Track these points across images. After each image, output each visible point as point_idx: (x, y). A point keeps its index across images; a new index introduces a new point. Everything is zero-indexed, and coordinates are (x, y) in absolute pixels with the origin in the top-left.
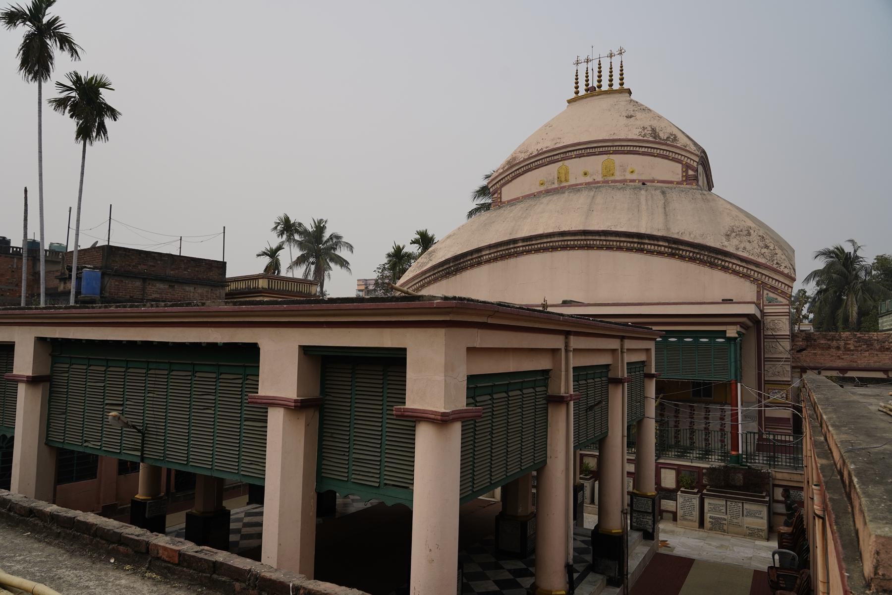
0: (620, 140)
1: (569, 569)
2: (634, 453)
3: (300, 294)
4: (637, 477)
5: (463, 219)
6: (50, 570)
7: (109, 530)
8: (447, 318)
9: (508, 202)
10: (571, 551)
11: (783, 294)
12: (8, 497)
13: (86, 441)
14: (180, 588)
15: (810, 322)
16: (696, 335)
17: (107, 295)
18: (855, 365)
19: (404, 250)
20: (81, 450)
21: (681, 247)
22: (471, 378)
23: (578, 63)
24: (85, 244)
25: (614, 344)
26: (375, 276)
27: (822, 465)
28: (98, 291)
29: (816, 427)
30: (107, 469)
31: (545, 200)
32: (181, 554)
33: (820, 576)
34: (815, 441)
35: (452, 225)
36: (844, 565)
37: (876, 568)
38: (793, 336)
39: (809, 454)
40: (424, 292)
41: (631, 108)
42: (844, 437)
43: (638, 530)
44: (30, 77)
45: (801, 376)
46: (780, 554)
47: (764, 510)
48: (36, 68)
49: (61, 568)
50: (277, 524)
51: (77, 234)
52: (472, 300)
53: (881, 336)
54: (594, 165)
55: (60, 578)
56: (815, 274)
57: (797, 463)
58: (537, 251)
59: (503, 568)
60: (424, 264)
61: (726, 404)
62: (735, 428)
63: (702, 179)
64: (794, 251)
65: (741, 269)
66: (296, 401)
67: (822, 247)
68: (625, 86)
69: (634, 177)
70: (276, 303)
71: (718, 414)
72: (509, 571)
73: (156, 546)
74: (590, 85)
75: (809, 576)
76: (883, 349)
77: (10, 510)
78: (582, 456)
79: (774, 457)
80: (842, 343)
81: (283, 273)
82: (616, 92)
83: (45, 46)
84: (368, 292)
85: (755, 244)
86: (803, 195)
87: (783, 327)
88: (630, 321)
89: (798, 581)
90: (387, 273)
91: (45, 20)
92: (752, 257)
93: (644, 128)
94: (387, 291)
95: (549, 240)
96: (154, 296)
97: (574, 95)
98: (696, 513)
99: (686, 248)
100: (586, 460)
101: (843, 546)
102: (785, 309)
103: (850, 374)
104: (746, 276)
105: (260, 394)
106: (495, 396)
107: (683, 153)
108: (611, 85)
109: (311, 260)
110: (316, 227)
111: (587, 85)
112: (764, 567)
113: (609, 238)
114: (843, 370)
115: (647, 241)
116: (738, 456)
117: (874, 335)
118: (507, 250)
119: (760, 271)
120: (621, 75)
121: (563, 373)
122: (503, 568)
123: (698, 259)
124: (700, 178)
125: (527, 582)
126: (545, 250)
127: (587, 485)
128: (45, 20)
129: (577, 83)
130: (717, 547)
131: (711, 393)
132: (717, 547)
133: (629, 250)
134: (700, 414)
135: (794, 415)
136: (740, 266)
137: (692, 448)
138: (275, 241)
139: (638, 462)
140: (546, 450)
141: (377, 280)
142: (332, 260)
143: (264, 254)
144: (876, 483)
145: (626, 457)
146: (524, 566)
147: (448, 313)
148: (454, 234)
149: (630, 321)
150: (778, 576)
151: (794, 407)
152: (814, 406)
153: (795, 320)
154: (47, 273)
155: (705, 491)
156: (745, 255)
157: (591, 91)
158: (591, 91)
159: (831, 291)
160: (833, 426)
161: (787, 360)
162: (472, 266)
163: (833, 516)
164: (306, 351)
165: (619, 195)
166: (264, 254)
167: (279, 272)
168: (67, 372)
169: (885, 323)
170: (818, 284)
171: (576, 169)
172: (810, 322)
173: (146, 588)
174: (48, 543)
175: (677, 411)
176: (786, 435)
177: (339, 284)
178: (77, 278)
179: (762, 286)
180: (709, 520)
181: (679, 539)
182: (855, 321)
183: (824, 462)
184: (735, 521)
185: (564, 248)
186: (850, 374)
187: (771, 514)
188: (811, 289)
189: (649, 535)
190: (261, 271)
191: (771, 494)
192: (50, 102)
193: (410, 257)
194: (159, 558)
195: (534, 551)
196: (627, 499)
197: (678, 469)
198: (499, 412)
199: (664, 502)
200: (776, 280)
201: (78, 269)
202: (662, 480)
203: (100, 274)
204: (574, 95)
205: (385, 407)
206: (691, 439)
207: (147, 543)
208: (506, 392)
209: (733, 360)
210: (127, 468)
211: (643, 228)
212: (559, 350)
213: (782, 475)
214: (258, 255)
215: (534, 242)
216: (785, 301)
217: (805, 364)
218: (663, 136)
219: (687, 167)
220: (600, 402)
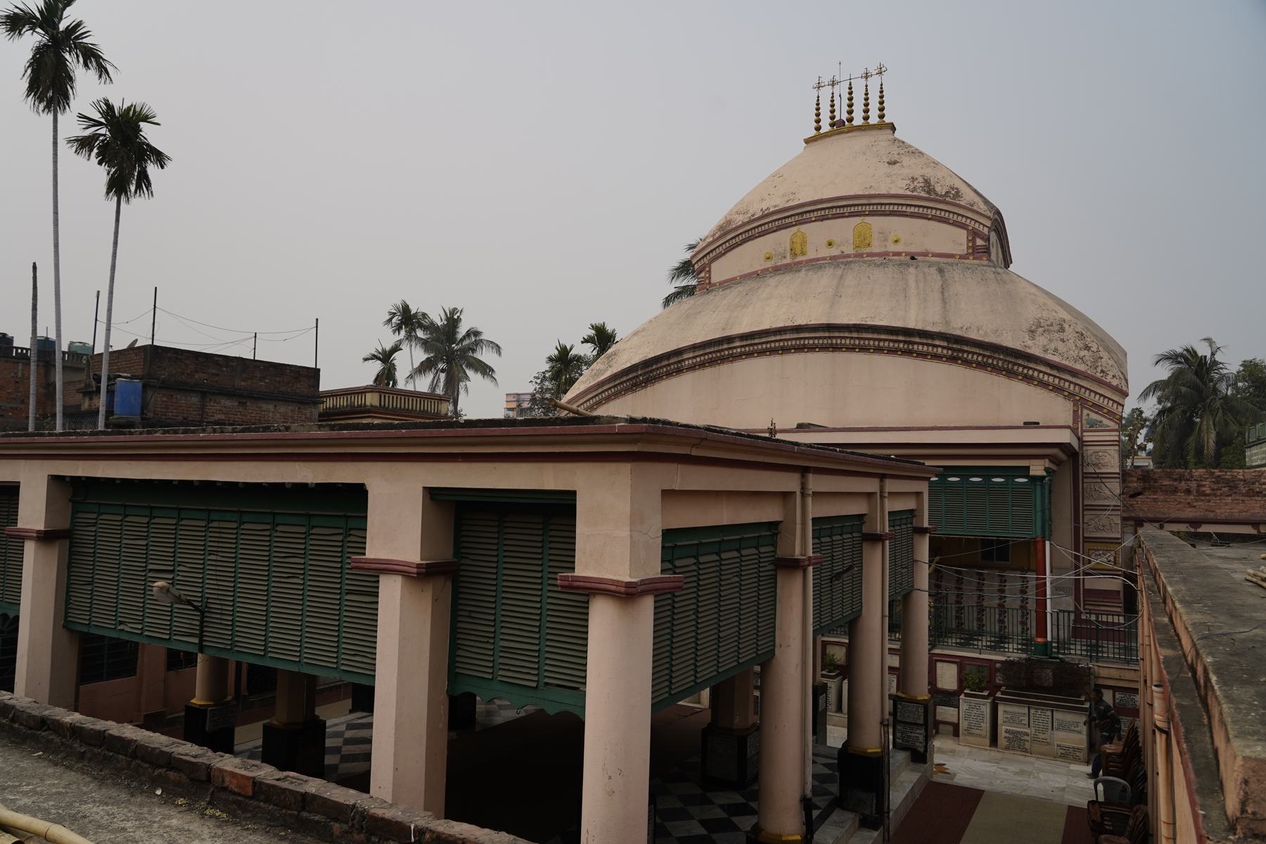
1: (807, 804)
2: (899, 640)
3: (423, 414)
5: (657, 308)
6: (70, 805)
7: (154, 749)
8: (634, 448)
9: (721, 283)
11: (1110, 414)
12: (11, 702)
13: (121, 623)
14: (255, 831)
15: (1149, 454)
17: (150, 415)
18: (1212, 515)
19: (573, 352)
20: (114, 635)
21: (965, 348)
22: (668, 534)
25: (871, 485)
26: (530, 389)
27: (1165, 657)
28: (138, 411)
30: (151, 662)
31: (772, 281)
32: (255, 783)
35: (641, 316)
36: (1197, 798)
37: (1243, 804)
38: (1125, 475)
39: (1147, 642)
40: (602, 412)
41: (895, 150)
42: (1198, 617)
43: (904, 749)
44: (42, 106)
45: (1136, 532)
48: (50, 94)
49: (86, 803)
51: (108, 330)
52: (670, 423)
53: (1249, 474)
54: (843, 231)
55: (85, 817)
56: (1156, 386)
57: (1129, 655)
58: (762, 353)
60: (600, 372)
61: (1029, 570)
62: (1042, 604)
63: (995, 252)
65: (1051, 379)
66: (419, 566)
67: (1165, 349)
68: (887, 120)
69: (899, 248)
71: (1018, 584)
72: (722, 807)
73: (221, 771)
74: (837, 118)
75: (1146, 815)
76: (1252, 494)
77: (13, 720)
78: (825, 644)
79: (1098, 646)
80: (1194, 485)
81: (401, 385)
82: (873, 127)
84: (522, 411)
85: (1071, 344)
86: (1138, 273)
87: (1111, 461)
89: (1131, 822)
90: (547, 384)
93: (913, 179)
94: (548, 410)
96: (218, 417)
97: (814, 132)
98: (986, 725)
100: (831, 650)
101: (1198, 773)
102: (1113, 436)
103: (1204, 529)
104: (1057, 390)
106: (702, 559)
107: (970, 215)
108: (866, 118)
109: (441, 366)
110: (448, 319)
111: (832, 118)
112: (1083, 802)
113: (864, 335)
115: (917, 340)
116: (1046, 643)
117: (1239, 474)
118: (718, 352)
119: (1078, 381)
120: (881, 103)
121: (798, 527)
123: (990, 365)
125: (746, 823)
126: (773, 351)
127: (832, 685)
129: (818, 115)
134: (991, 585)
135: (1126, 587)
136: (1050, 375)
137: (980, 632)
138: (389, 338)
139: (904, 653)
142: (470, 366)
143: (374, 357)
146: (743, 801)
147: (635, 442)
148: (643, 330)
150: (1103, 815)
151: (1126, 575)
152: (1154, 574)
153: (1127, 451)
154: (65, 384)
155: (999, 695)
156: (1056, 359)
157: (839, 127)
158: (839, 127)
159: (1178, 411)
160: (1181, 601)
161: (1115, 508)
162: (669, 375)
163: (1182, 730)
164: (434, 495)
165: (877, 274)
166: (374, 357)
167: (395, 383)
168: (94, 525)
169: (1255, 456)
170: (1159, 403)
171: (817, 237)
172: (1149, 454)
173: (206, 831)
174: (67, 767)
175: (959, 581)
176: (1114, 614)
177: (481, 400)
178: (108, 392)
179: (1080, 403)
180: (1004, 734)
181: (963, 762)
183: (1169, 652)
184: (1041, 736)
185: (800, 349)
186: (1204, 529)
188: (1151, 408)
189: (920, 757)
190: (368, 380)
192: (69, 142)
193: (578, 359)
194: (225, 789)
195: (756, 778)
196: (889, 705)
197: (961, 663)
198: (707, 581)
201: (109, 379)
202: (939, 679)
203: (140, 385)
204: (814, 132)
205: (546, 575)
206: (980, 620)
207: (209, 767)
208: (757, 548)
209: (1039, 508)
210: (179, 660)
211: (912, 321)
212: (792, 494)
214: (366, 360)
215: (757, 341)
216: (1113, 425)
217: (1141, 515)
220: (851, 568)
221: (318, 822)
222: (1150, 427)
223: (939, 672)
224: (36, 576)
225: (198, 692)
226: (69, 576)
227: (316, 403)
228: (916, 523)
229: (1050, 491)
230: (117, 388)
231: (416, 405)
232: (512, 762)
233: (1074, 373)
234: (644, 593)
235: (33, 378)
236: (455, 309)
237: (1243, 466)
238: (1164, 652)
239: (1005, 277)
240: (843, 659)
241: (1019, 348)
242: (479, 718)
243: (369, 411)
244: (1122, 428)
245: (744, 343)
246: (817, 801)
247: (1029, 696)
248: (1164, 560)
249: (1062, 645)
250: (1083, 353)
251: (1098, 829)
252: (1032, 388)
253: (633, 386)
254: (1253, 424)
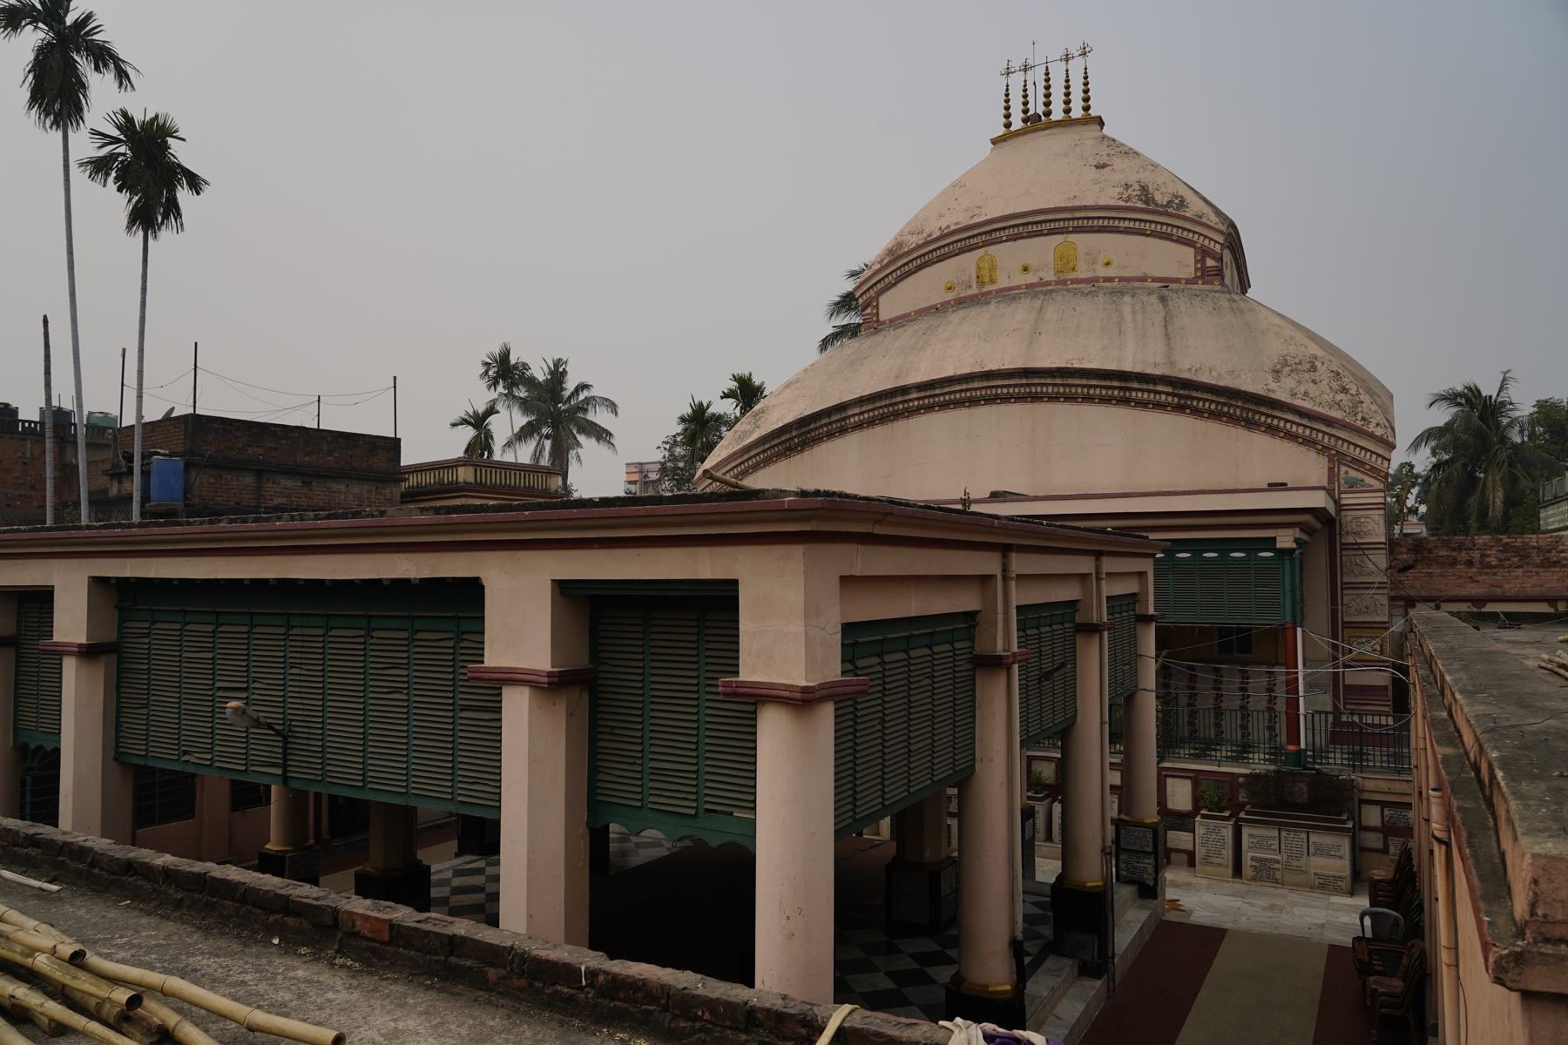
0: (1085, 208)
1: (1016, 948)
2: (1120, 752)
3: (530, 491)
4: (1125, 793)
5: (813, 355)
6: (175, 958)
7: (267, 892)
8: (808, 527)
9: (891, 321)
10: (1020, 918)
11: (1374, 472)
12: (88, 844)
13: (185, 753)
14: (395, 981)
15: (1421, 518)
16: (1224, 546)
17: (196, 500)
18: (1498, 591)
19: (710, 410)
20: (177, 767)
21: (1195, 394)
22: (848, 628)
23: (1008, 73)
24: (153, 413)
25: (1085, 565)
26: (659, 456)
27: (1444, 756)
28: (180, 495)
29: (1434, 696)
30: (213, 798)
31: (955, 317)
32: (393, 927)
33: (1445, 957)
34: (1432, 719)
35: (793, 362)
36: (1482, 906)
37: (1533, 906)
38: (1392, 545)
39: (1421, 745)
40: (756, 481)
41: (1104, 150)
42: (1481, 708)
43: (1129, 882)
44: (48, 123)
45: (1406, 613)
46: (1373, 916)
47: (1345, 844)
48: (57, 106)
49: (193, 955)
50: (524, 883)
51: (140, 397)
52: (847, 496)
53: (1544, 540)
54: (1041, 253)
55: (195, 970)
56: (1429, 435)
57: (1400, 763)
58: (944, 406)
59: (900, 951)
60: (746, 434)
61: (1277, 664)
62: (1293, 704)
63: (1230, 274)
64: (1391, 397)
65: (1301, 430)
66: (550, 674)
67: (1443, 387)
68: (1093, 112)
69: (1110, 272)
70: (511, 508)
71: (1264, 680)
72: (912, 956)
73: (351, 914)
75: (1423, 952)
76: (1548, 564)
77: (92, 865)
78: (1030, 759)
79: (1361, 753)
80: (1476, 555)
81: (497, 457)
82: (1077, 122)
83: (72, 66)
84: (646, 483)
85: (1324, 386)
86: (1404, 301)
87: (1375, 528)
88: (1109, 525)
89: (1405, 960)
90: (679, 451)
91: (69, 20)
92: (1320, 409)
93: (1127, 187)
94: (679, 483)
96: (278, 501)
97: (1002, 131)
98: (1228, 853)
99: (1205, 396)
100: (1038, 767)
101: (1482, 878)
102: (1378, 498)
103: (1490, 608)
104: (1309, 443)
105: (487, 664)
106: (887, 658)
107: (1198, 229)
108: (1067, 111)
109: (545, 431)
110: (551, 373)
111: (1025, 111)
112: (1347, 940)
113: (1071, 381)
114: (1479, 601)
115: (1136, 385)
116: (1299, 752)
117: (1533, 540)
118: (891, 406)
119: (1334, 432)
121: (1000, 617)
122: (900, 951)
123: (1225, 414)
124: (1227, 273)
125: (943, 974)
126: (958, 404)
127: (1040, 809)
128: (69, 20)
129: (1007, 108)
130: (1265, 909)
131: (1253, 645)
132: (1265, 909)
134: (1231, 682)
135: (1395, 680)
136: (1299, 425)
137: (1218, 741)
138: (481, 395)
139: (1128, 768)
140: (974, 749)
141: (663, 464)
142: (582, 430)
143: (464, 422)
144: (1537, 777)
145: (1109, 760)
146: (938, 948)
147: (808, 519)
148: (798, 380)
149: (1109, 525)
150: (1370, 953)
151: (1394, 666)
152: (1429, 662)
153: (1394, 516)
154: (89, 463)
155: (1242, 815)
156: (1307, 405)
157: (1033, 122)
158: (1033, 122)
159: (1458, 465)
160: (1462, 692)
161: (1381, 586)
162: (830, 435)
163: (1464, 834)
164: (565, 590)
165: (1084, 305)
166: (464, 422)
167: (491, 453)
168: (147, 635)
169: (1552, 517)
170: (1434, 453)
172: (1421, 518)
173: (339, 982)
174: (162, 917)
175: (1192, 678)
176: (1380, 715)
177: (596, 474)
178: (143, 473)
179: (1337, 459)
180: (1250, 862)
181: (1200, 897)
182: (1499, 514)
183: (1449, 750)
184: (1295, 863)
185: (991, 400)
186: (1490, 608)
187: (1357, 850)
188: (1423, 461)
189: (1149, 891)
190: (458, 452)
191: (1356, 817)
192: (81, 165)
193: (719, 420)
194: (355, 935)
195: (954, 921)
196: (1110, 829)
197: (1196, 778)
198: (895, 686)
199: (1172, 834)
200: (1362, 448)
201: (143, 457)
202: (1169, 798)
203: (182, 464)
204: (1002, 131)
205: (703, 681)
206: (1217, 725)
207: (335, 911)
208: (930, 647)
209: (1288, 588)
210: (248, 796)
211: (1129, 362)
212: (992, 577)
213: (1374, 783)
214: (454, 425)
216: (1377, 484)
217: (1412, 593)
218: (1161, 198)
219: (1204, 252)
220: (1063, 665)
221: (470, 968)
222: (1421, 485)
223: (1169, 789)
224: (79, 699)
225: (273, 836)
226: (118, 698)
227: (397, 481)
228: (1139, 610)
229: (1301, 568)
230: (154, 468)
231: (520, 481)
232: (680, 901)
233: (1329, 422)
234: (823, 699)
235: (49, 458)
236: (560, 360)
237: (1536, 530)
238: (1442, 751)
239: (1242, 305)
240: (1053, 777)
241: (1261, 392)
242: (612, 858)
243: (462, 489)
244: (1389, 487)
245: (923, 394)
246: (1028, 947)
247: (1278, 816)
248: (1443, 645)
249: (1319, 753)
250: (1340, 397)
251: (1365, 969)
252: (1278, 441)
254: (1549, 479)
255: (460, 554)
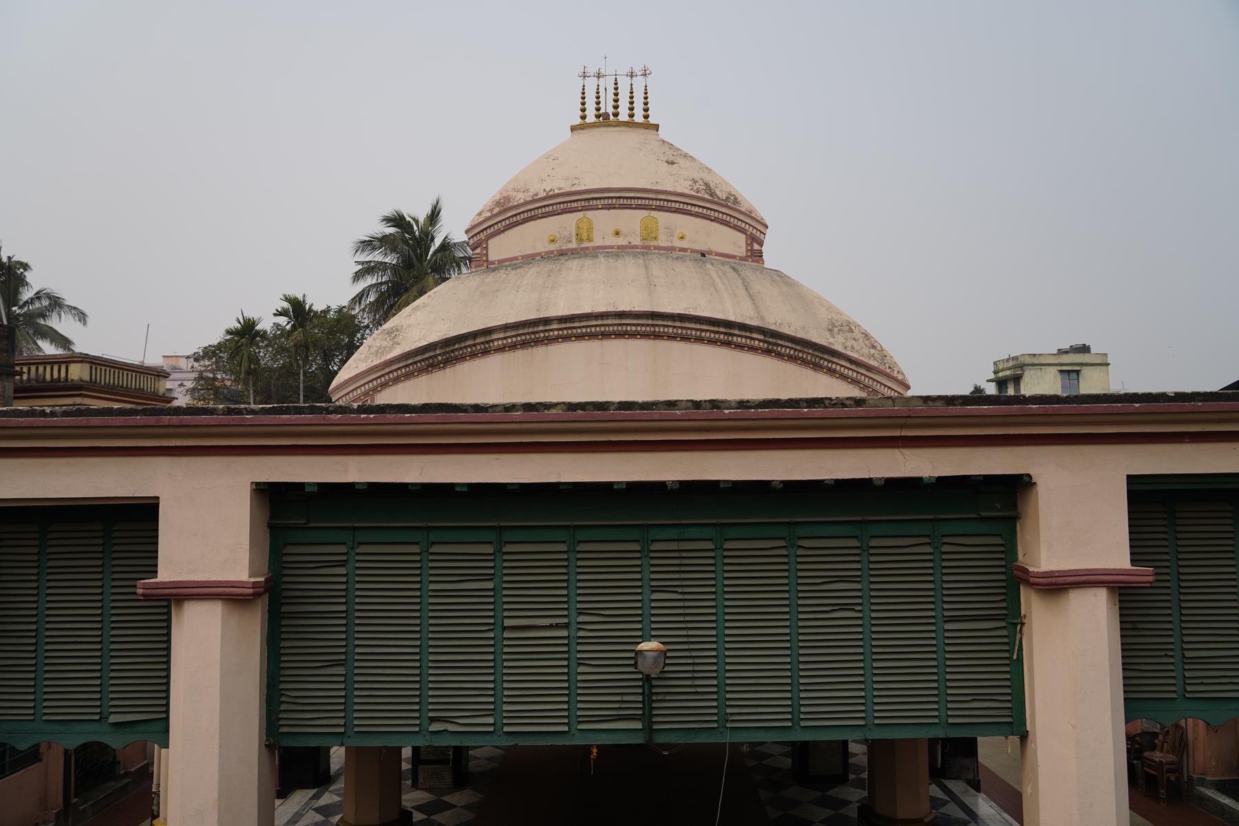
3: (139, 394)
9: (500, 262)
13: (432, 720)
21: (780, 342)
54: (631, 222)
58: (580, 337)
68: (652, 120)
69: (684, 244)
93: (695, 182)
95: (600, 322)
97: (579, 121)
107: (753, 223)
108: (631, 116)
111: (598, 109)
115: (737, 332)
119: (872, 375)
120: (646, 104)
122: (465, 807)
123: (800, 358)
126: (592, 336)
133: (711, 342)
157: (604, 120)
162: (473, 356)
168: (343, 564)
171: (606, 225)
185: (620, 335)
204: (579, 121)
215: (576, 325)
233: (869, 368)
245: (563, 326)
250: (873, 351)
253: (428, 366)
255: (1074, 447)
